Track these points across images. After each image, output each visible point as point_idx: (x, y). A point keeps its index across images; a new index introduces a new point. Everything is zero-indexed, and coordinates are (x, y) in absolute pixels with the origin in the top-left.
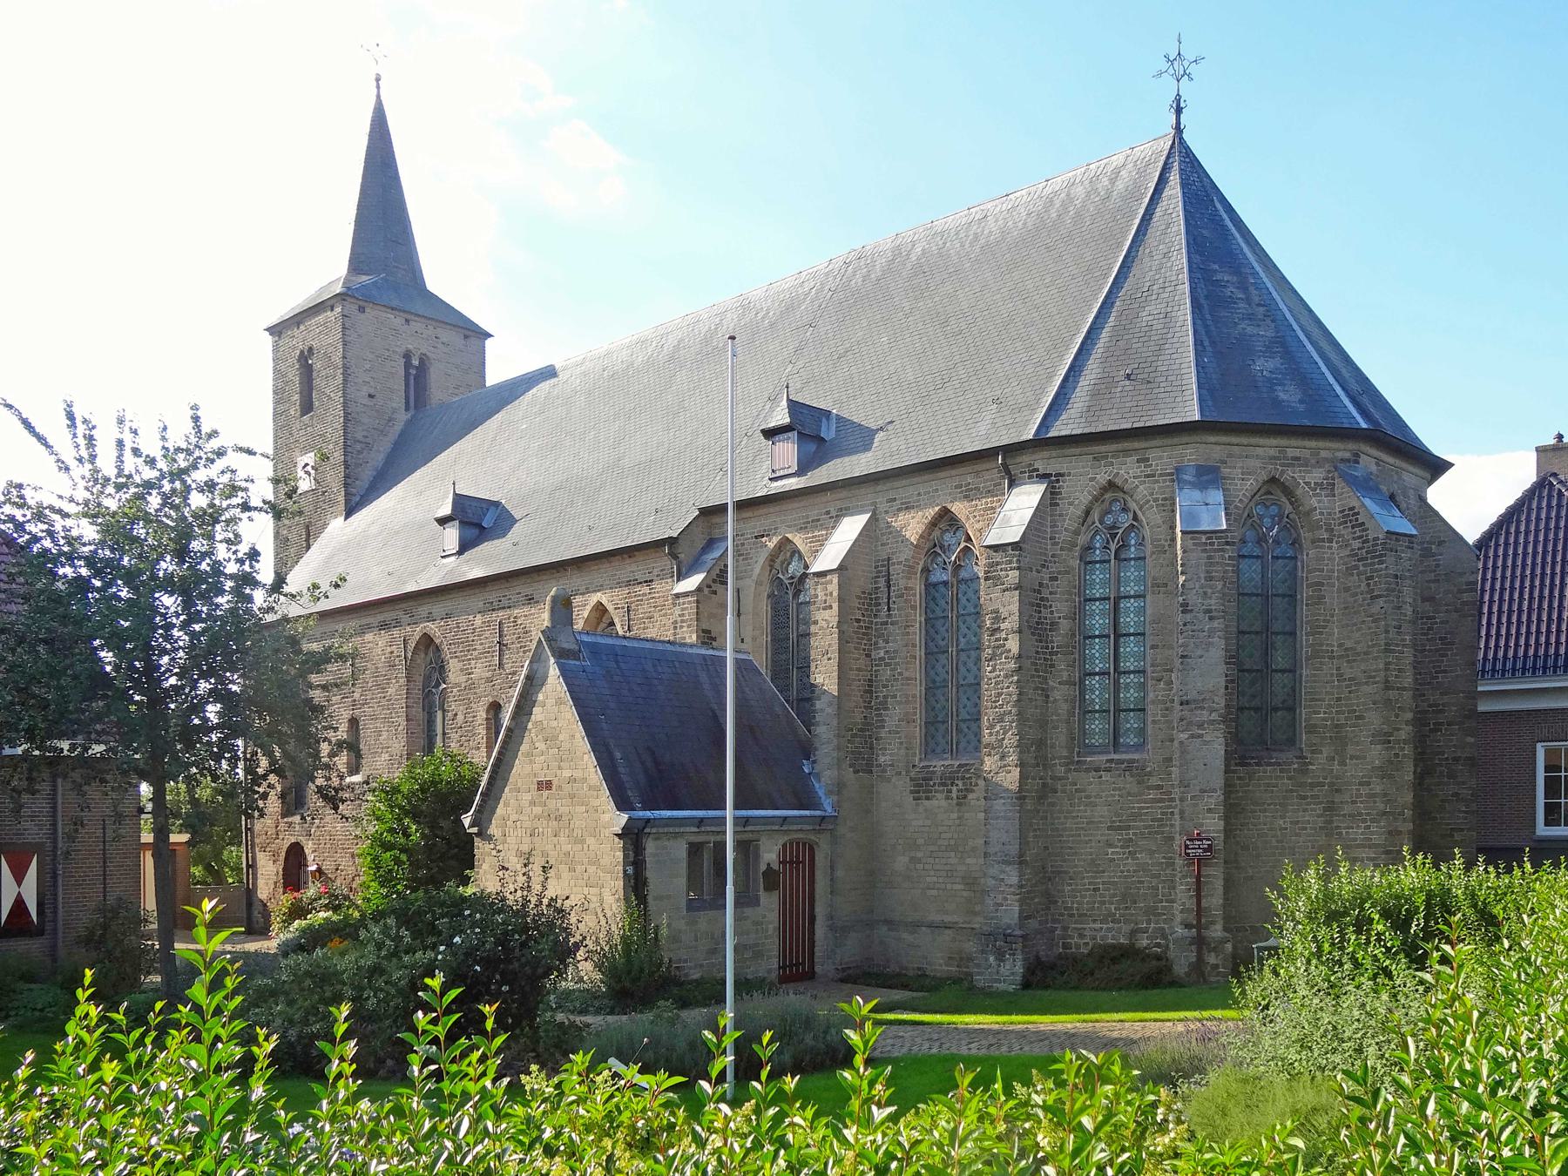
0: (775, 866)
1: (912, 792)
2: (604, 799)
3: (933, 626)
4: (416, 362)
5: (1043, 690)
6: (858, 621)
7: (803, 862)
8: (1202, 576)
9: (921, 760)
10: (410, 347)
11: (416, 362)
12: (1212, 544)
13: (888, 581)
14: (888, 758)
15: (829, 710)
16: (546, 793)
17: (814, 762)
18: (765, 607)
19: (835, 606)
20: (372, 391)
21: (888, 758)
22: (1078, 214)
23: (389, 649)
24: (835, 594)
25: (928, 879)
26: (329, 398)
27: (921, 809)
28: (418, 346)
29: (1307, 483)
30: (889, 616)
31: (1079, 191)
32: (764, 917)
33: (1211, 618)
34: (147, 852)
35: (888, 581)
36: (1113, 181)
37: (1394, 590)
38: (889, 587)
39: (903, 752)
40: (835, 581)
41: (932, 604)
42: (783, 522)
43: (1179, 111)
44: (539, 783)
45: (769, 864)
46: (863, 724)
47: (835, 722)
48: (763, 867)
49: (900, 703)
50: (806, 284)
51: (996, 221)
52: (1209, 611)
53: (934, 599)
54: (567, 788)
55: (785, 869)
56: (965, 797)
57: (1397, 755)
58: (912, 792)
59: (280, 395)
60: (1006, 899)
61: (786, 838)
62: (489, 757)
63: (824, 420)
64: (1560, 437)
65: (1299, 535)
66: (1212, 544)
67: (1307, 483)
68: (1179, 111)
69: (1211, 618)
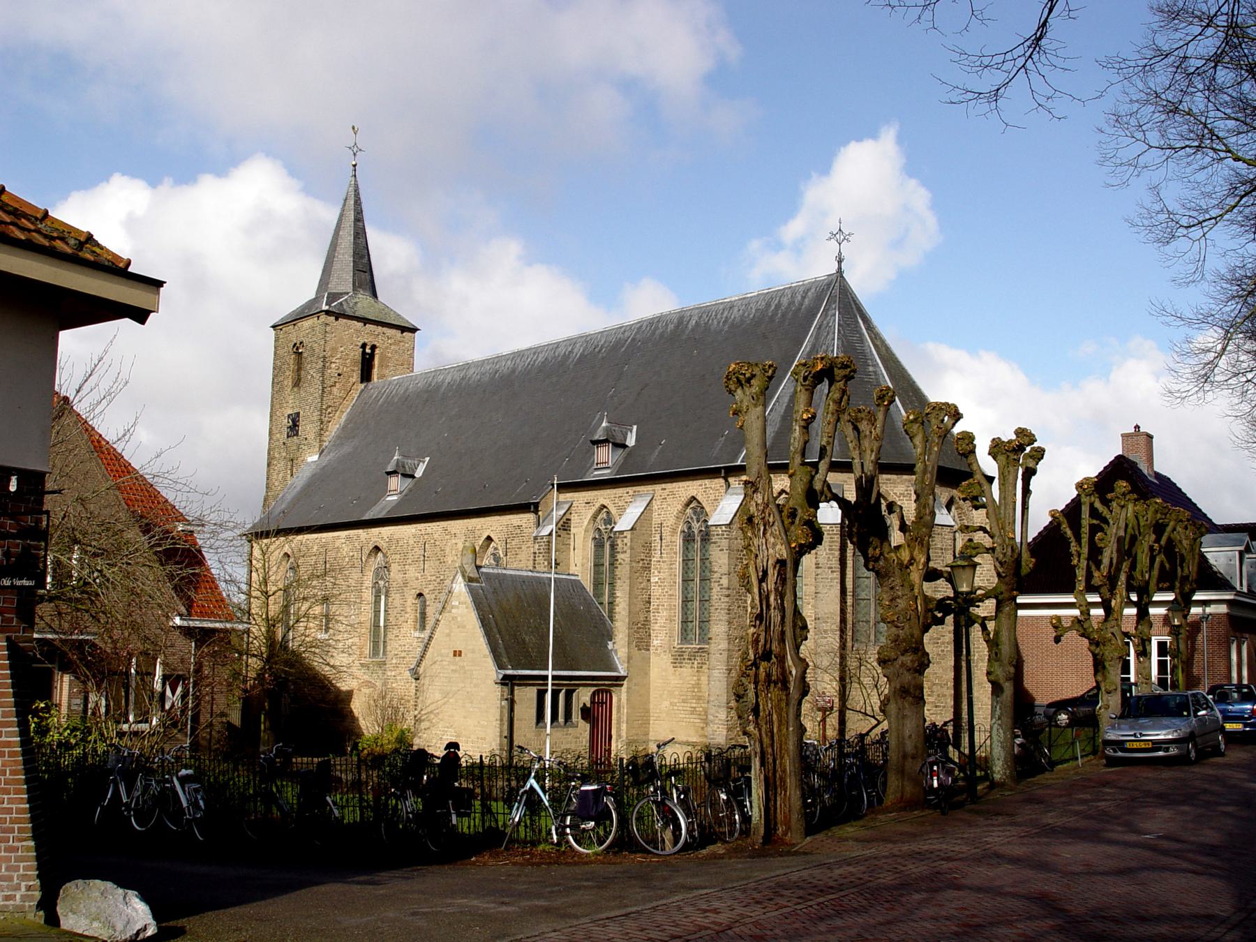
0: (588, 705)
1: (672, 663)
2: (490, 662)
3: (687, 564)
4: (368, 351)
5: (744, 607)
6: (643, 560)
7: (606, 703)
8: (827, 548)
9: (678, 644)
10: (366, 341)
11: (368, 351)
12: (833, 531)
13: (661, 537)
14: (659, 642)
15: (623, 613)
16: (457, 658)
17: (614, 643)
18: (590, 545)
19: (628, 551)
20: (340, 371)
21: (659, 642)
22: (783, 315)
23: (351, 554)
24: (629, 544)
25: (681, 716)
26: (312, 376)
27: (677, 673)
28: (370, 340)
29: (896, 494)
30: (661, 557)
31: (785, 301)
32: (581, 734)
33: (832, 572)
34: (65, 675)
35: (661, 537)
36: (803, 298)
37: (940, 557)
38: (661, 540)
39: (667, 638)
40: (629, 537)
41: (686, 552)
42: (601, 495)
43: (840, 262)
44: (455, 652)
45: (584, 704)
46: (644, 621)
47: (627, 621)
48: (581, 705)
49: (666, 609)
50: (626, 334)
51: (739, 310)
52: (831, 568)
53: (687, 549)
54: (470, 655)
55: (594, 708)
56: (701, 667)
57: (943, 651)
58: (672, 663)
59: (277, 371)
60: (718, 728)
61: (595, 688)
62: (661, 836)
63: (629, 433)
64: (1137, 427)
65: (892, 522)
66: (833, 531)
67: (896, 494)
68: (840, 262)
69: (832, 572)
